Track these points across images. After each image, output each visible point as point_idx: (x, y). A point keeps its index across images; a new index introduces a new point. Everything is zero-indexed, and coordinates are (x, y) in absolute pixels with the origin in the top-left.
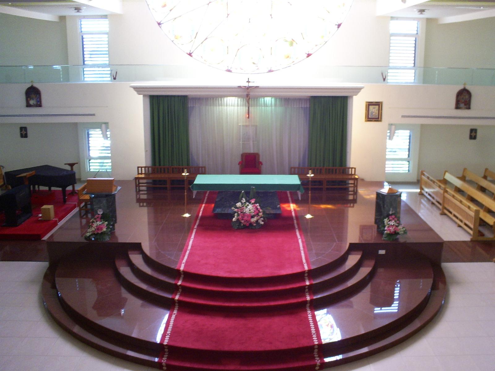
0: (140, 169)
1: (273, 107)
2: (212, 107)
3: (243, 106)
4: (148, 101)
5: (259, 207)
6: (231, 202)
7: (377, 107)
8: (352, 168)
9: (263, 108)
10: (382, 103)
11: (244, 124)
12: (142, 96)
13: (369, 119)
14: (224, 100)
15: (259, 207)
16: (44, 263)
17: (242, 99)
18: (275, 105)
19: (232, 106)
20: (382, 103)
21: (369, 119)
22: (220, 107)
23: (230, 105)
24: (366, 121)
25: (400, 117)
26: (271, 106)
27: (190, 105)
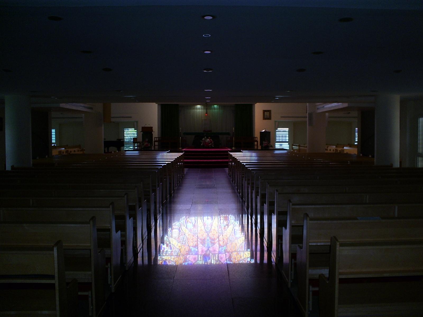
0: (156, 138)
1: (218, 110)
3: (204, 109)
4: (160, 107)
5: (212, 140)
8: (256, 137)
9: (213, 110)
10: (271, 110)
12: (157, 104)
13: (265, 118)
15: (212, 140)
16: (120, 262)
18: (219, 108)
20: (271, 110)
21: (265, 118)
22: (194, 110)
24: (263, 119)
25: (280, 117)
26: (217, 109)
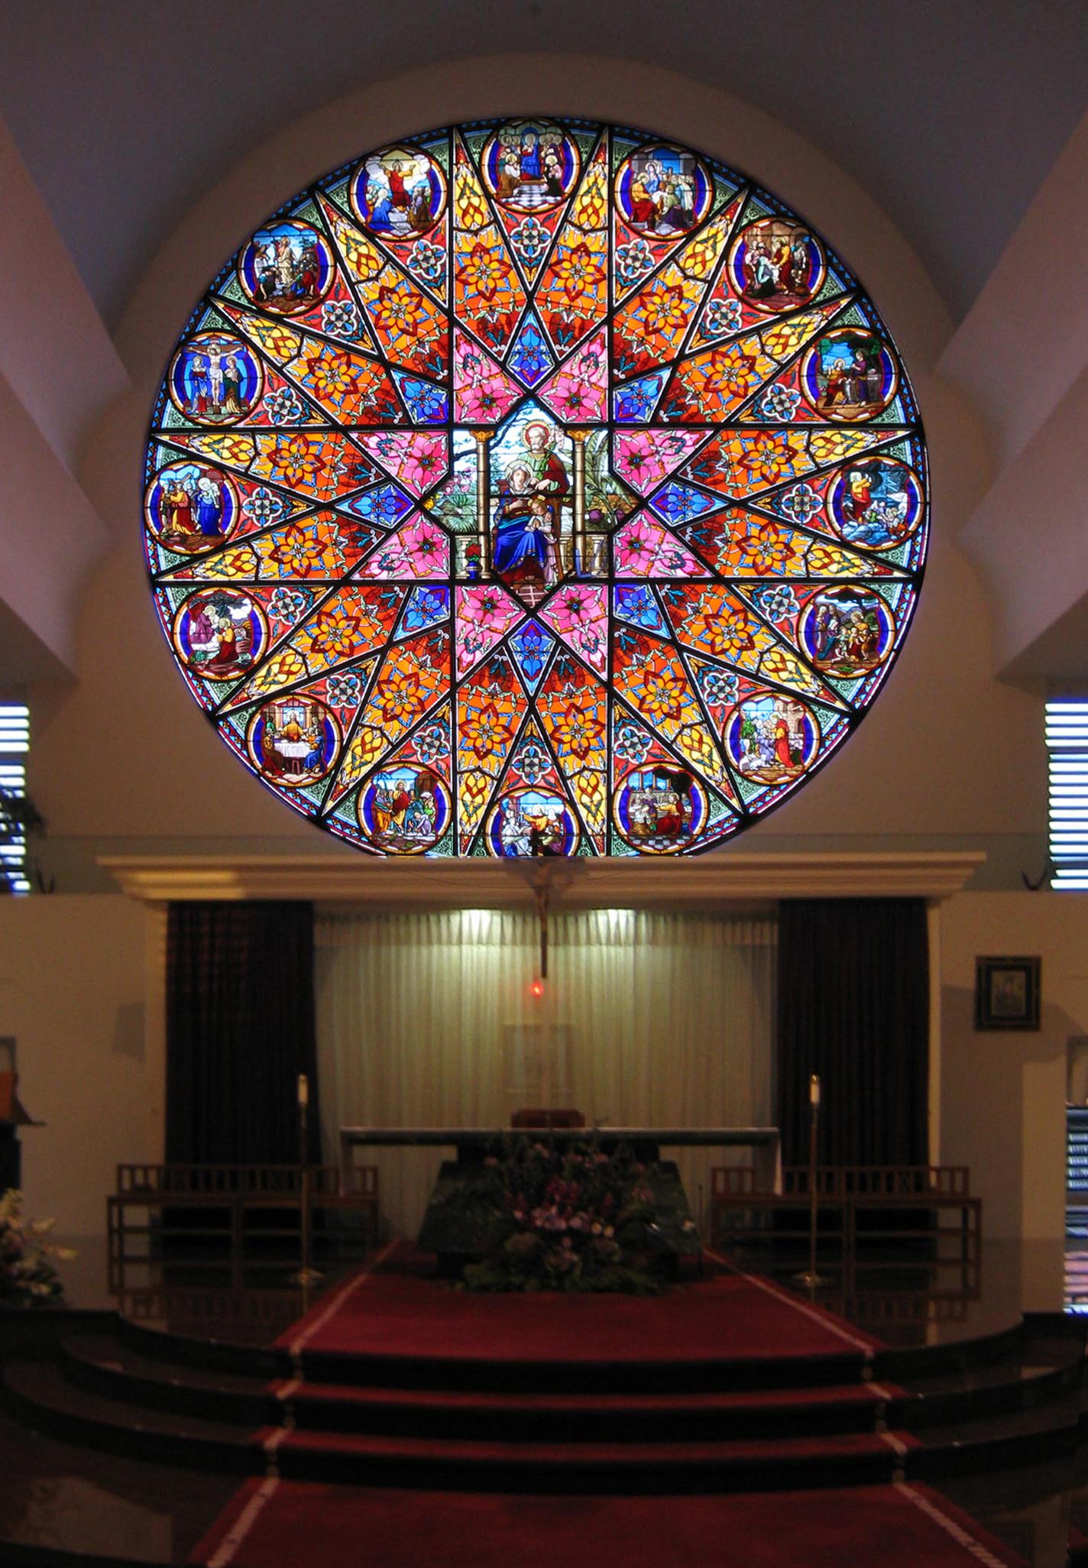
2: (404, 949)
6: (591, 1209)
7: (1020, 977)
9: (604, 948)
11: (531, 1021)
14: (449, 920)
17: (519, 920)
19: (480, 942)
23: (475, 938)
27: (321, 935)
